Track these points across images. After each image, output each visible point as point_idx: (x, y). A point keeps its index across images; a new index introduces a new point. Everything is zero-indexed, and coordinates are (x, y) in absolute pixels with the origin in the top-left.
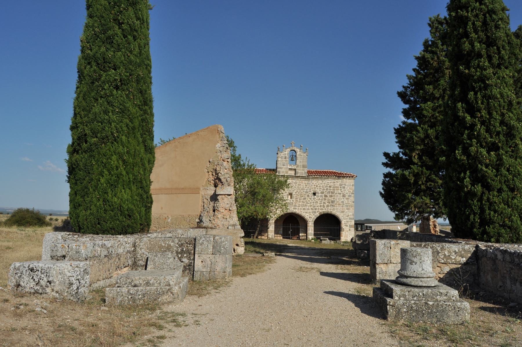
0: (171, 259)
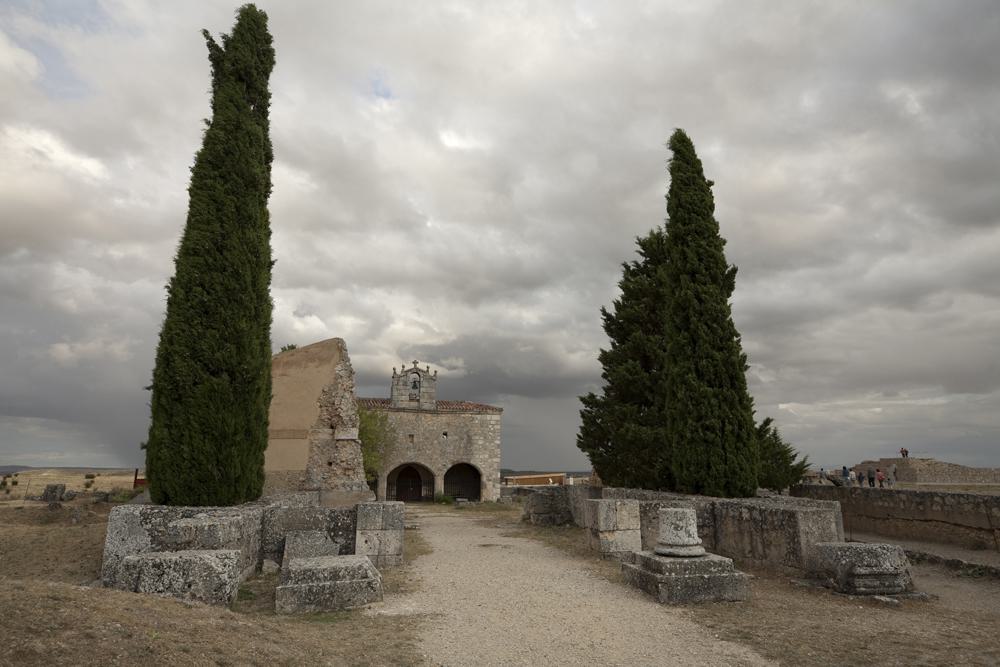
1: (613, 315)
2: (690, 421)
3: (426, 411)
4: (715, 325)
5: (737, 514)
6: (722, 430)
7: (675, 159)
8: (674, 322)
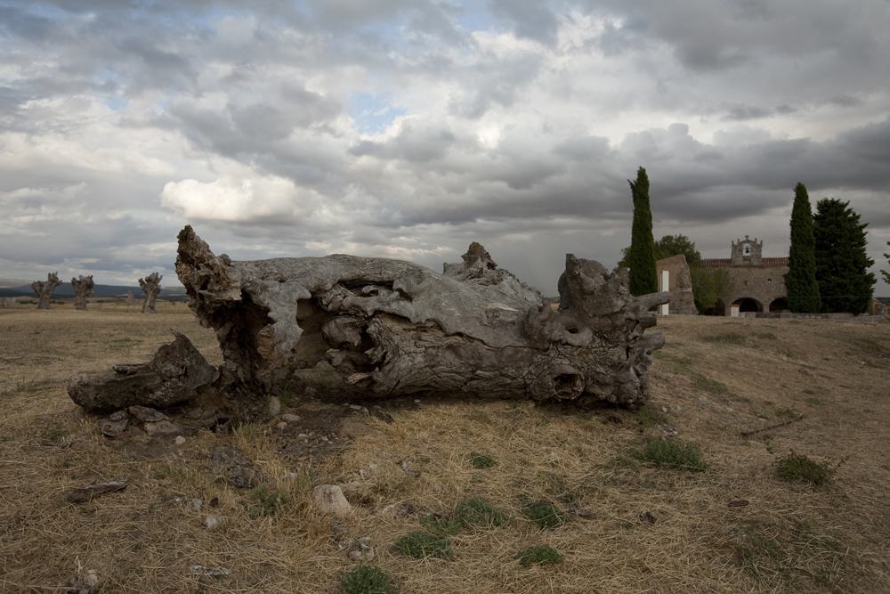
3: (756, 267)
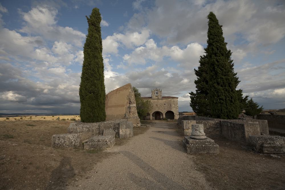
0: (111, 131)
1: (197, 70)
2: (215, 97)
3: (160, 99)
4: (223, 69)
5: (227, 125)
6: (226, 99)
7: (210, 21)
8: (210, 69)
